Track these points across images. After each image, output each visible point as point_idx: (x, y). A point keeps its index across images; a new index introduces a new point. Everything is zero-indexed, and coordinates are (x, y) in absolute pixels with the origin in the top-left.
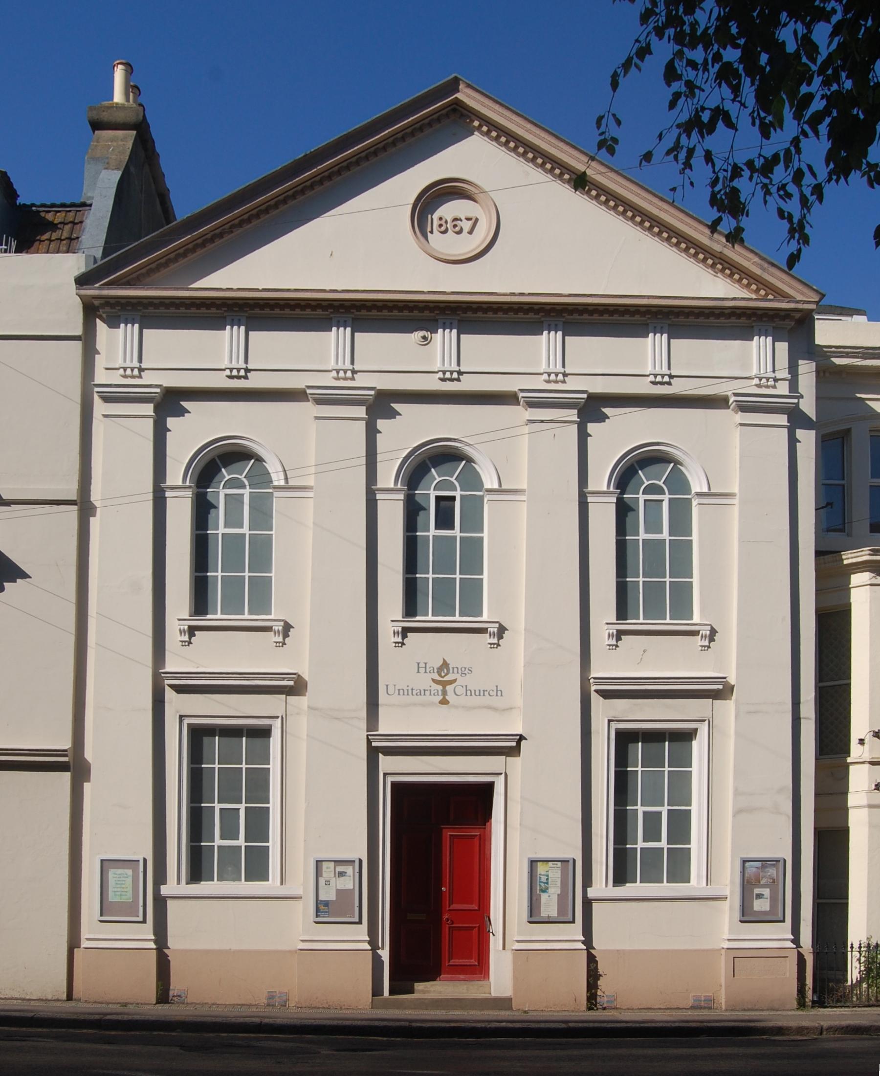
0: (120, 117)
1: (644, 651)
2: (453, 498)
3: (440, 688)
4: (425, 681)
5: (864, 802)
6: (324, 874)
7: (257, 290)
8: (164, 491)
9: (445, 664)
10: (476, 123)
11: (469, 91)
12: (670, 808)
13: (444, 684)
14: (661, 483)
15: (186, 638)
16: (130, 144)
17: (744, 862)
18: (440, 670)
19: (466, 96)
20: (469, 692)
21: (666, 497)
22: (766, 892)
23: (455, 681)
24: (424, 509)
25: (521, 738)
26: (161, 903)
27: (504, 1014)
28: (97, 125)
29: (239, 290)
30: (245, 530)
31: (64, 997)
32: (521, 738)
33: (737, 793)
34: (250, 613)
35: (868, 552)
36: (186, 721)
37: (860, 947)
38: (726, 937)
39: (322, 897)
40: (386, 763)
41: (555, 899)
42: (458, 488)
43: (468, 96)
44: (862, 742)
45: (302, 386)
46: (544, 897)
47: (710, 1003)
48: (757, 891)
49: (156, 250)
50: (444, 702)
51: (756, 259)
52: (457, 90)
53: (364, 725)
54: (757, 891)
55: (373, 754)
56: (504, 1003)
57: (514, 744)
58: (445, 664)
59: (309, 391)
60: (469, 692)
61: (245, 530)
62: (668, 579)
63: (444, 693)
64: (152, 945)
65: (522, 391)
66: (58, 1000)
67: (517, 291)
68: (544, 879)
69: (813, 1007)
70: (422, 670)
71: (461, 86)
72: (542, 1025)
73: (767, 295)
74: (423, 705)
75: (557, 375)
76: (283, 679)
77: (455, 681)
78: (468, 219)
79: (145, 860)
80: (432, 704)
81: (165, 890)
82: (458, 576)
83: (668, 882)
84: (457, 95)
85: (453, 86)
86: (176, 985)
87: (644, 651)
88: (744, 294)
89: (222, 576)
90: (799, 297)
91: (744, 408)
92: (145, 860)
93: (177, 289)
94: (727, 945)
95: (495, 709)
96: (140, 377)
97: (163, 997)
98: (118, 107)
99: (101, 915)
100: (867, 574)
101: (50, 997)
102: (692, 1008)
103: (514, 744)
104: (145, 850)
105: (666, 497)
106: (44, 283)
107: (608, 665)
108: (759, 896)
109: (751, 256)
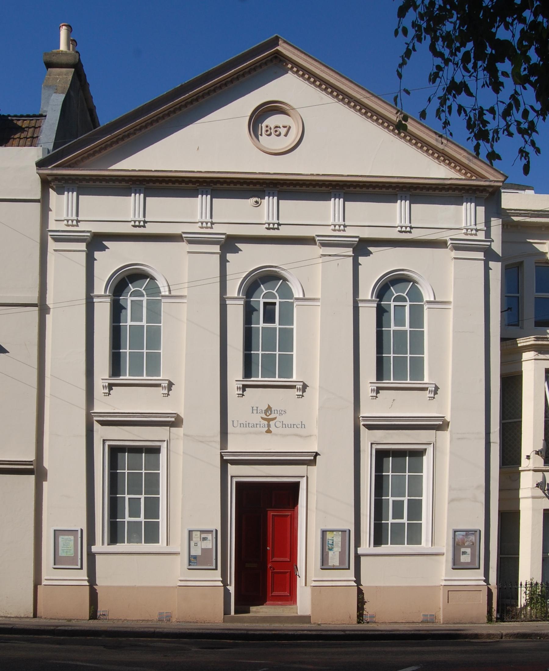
0: (64, 60)
1: (394, 400)
2: (274, 304)
3: (266, 423)
4: (257, 418)
5: (530, 495)
6: (194, 539)
7: (193, 172)
8: (93, 298)
9: (269, 408)
10: (290, 66)
11: (285, 45)
12: (409, 498)
13: (269, 420)
14: (404, 295)
15: (107, 391)
16: (70, 77)
17: (455, 531)
18: (266, 412)
19: (283, 48)
20: (284, 425)
21: (408, 304)
22: (469, 550)
23: (275, 418)
24: (256, 310)
25: (317, 454)
26: (92, 557)
27: (306, 626)
28: (49, 65)
29: (140, 171)
30: (144, 323)
31: (32, 615)
32: (317, 454)
33: (450, 489)
34: (147, 375)
35: (533, 339)
36: (107, 443)
37: (526, 585)
38: (444, 578)
39: (193, 553)
40: (232, 470)
41: (337, 554)
42: (145, 296)
43: (285, 48)
44: (528, 457)
45: (179, 232)
46: (331, 553)
47: (433, 619)
48: (463, 550)
49: (86, 145)
50: (269, 431)
51: (465, 154)
52: (278, 45)
53: (219, 446)
54: (463, 550)
55: (224, 464)
56: (306, 619)
57: (312, 458)
58: (269, 408)
59: (317, 238)
60: (284, 425)
61: (144, 323)
62: (408, 355)
63: (269, 426)
64: (87, 583)
65: (318, 236)
66: (28, 617)
67: (315, 173)
68: (330, 542)
69: (496, 622)
70: (255, 412)
71: (280, 42)
72: (329, 633)
73: (472, 176)
74: (255, 433)
75: (207, 223)
76: (168, 417)
77: (275, 418)
78: (284, 127)
79: (82, 530)
80: (261, 433)
81: (94, 549)
82: (277, 353)
83: (391, 544)
84: (278, 48)
85: (275, 42)
86: (101, 608)
87: (394, 400)
88: (458, 176)
89: (146, 352)
90: (492, 178)
91: (457, 248)
92: (82, 530)
93: (101, 170)
94: (444, 583)
95: (301, 436)
96: (77, 226)
97: (94, 615)
98: (63, 53)
99: (55, 565)
100: (533, 352)
101: (22, 616)
102: (422, 622)
103: (312, 458)
104: (82, 524)
105: (408, 304)
106: (16, 166)
107: (370, 409)
108: (464, 553)
109: (462, 152)
